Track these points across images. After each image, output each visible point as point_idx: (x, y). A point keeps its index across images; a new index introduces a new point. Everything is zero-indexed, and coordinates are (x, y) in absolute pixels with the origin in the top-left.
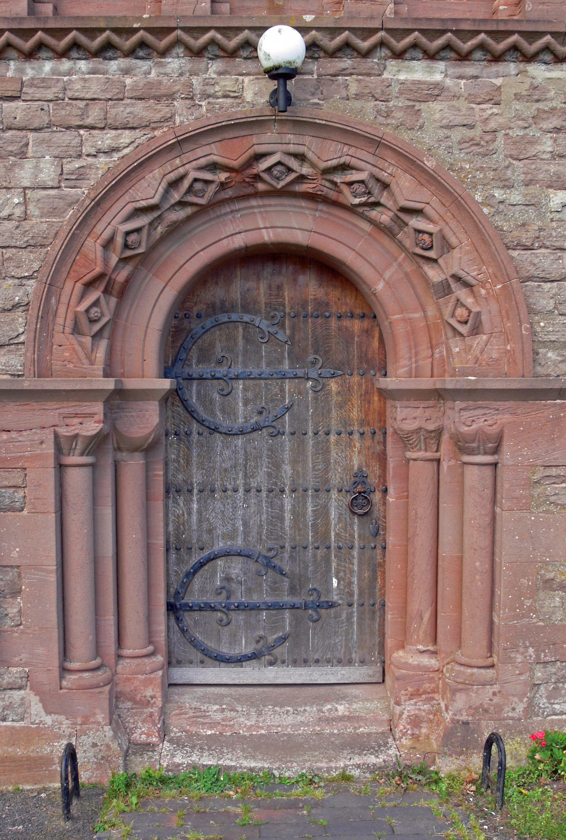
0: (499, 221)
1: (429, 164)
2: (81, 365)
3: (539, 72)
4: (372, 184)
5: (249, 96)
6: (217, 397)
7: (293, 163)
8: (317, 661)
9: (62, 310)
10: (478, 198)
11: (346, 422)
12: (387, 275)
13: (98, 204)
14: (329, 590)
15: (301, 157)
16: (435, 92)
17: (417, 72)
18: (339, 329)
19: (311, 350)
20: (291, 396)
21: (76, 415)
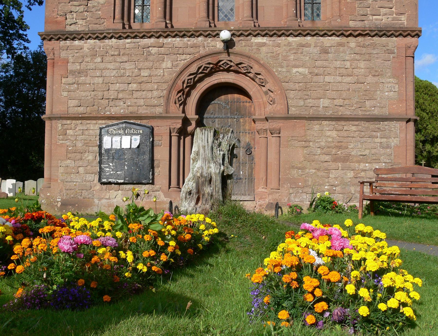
0: (279, 76)
1: (262, 62)
2: (175, 110)
3: (290, 39)
4: (248, 67)
5: (218, 46)
6: (211, 123)
7: (229, 62)
8: (237, 194)
9: (172, 98)
10: (274, 70)
11: (245, 130)
12: (253, 90)
13: (181, 72)
14: (240, 175)
15: (231, 61)
16: (264, 44)
17: (260, 40)
18: (243, 105)
19: (235, 111)
20: (230, 123)
21: (175, 123)
